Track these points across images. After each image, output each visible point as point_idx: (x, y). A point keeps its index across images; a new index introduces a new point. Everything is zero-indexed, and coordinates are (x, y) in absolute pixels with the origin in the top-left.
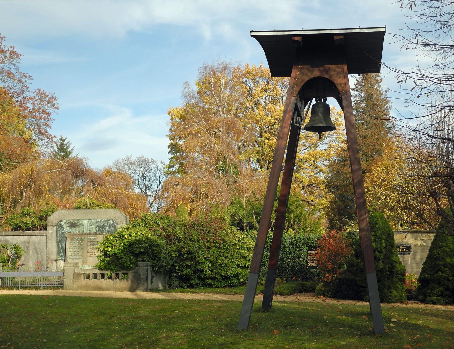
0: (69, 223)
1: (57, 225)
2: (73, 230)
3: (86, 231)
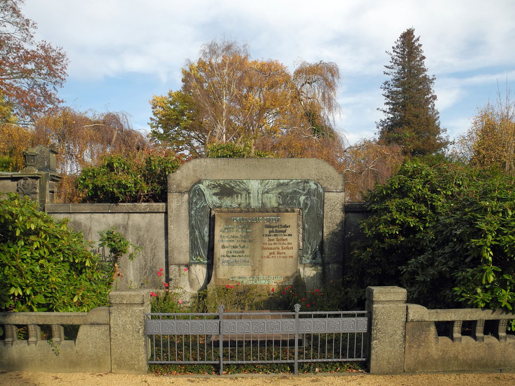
0: (216, 187)
1: (189, 192)
2: (227, 202)
3: (254, 204)
